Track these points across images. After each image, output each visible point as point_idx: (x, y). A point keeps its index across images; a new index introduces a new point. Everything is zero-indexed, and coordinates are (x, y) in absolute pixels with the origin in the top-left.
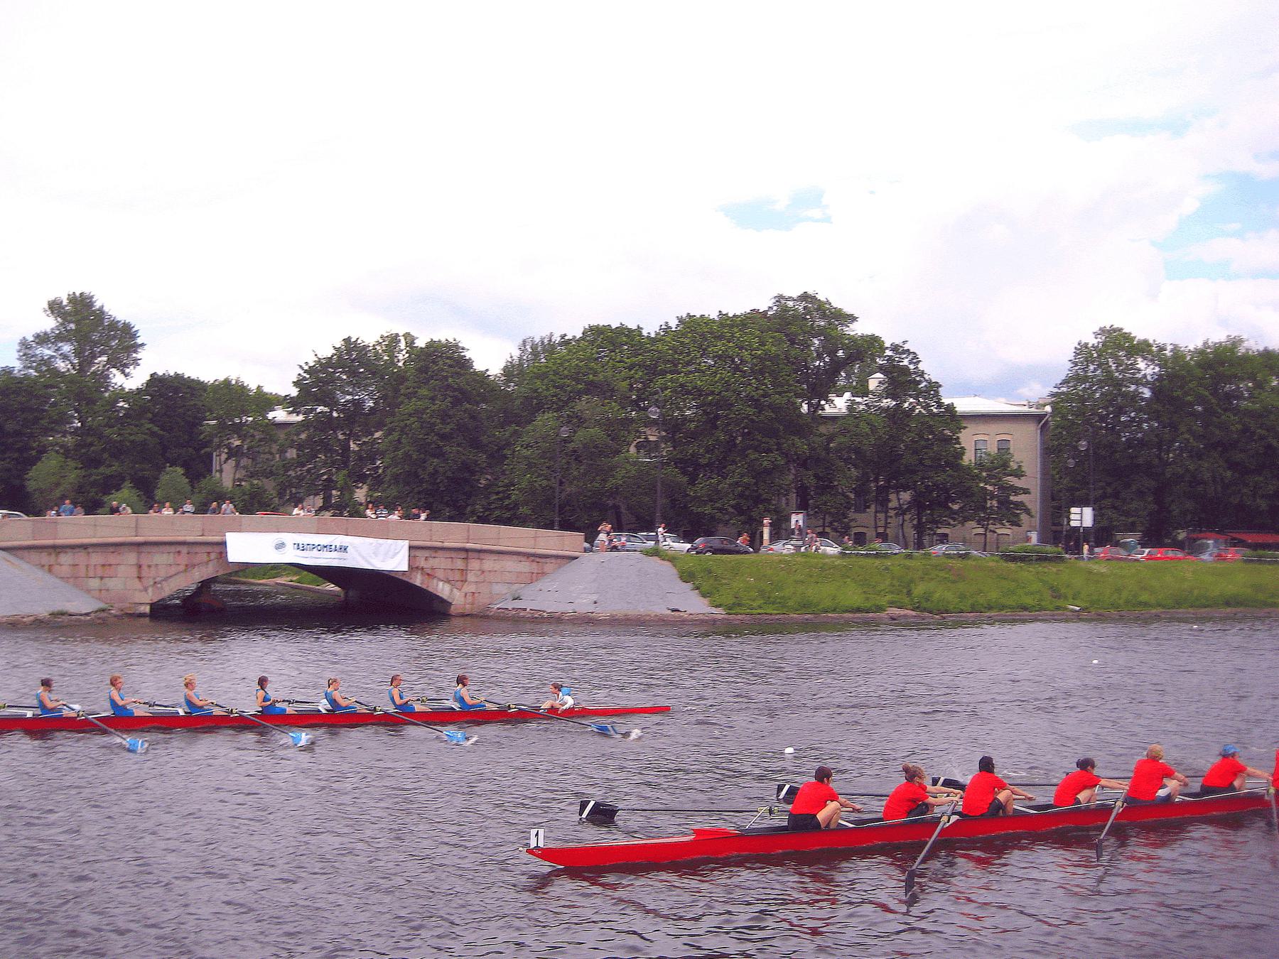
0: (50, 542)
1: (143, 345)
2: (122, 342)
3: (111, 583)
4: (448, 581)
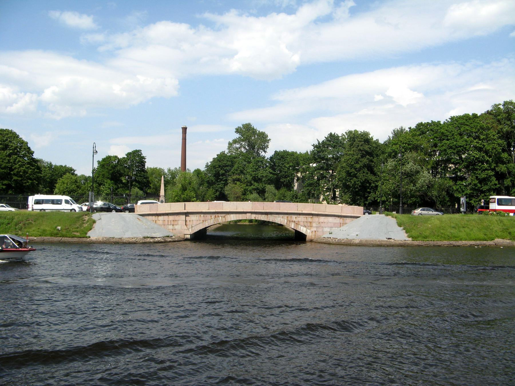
0: (155, 212)
1: (270, 140)
2: (263, 140)
3: (176, 227)
4: (305, 227)
